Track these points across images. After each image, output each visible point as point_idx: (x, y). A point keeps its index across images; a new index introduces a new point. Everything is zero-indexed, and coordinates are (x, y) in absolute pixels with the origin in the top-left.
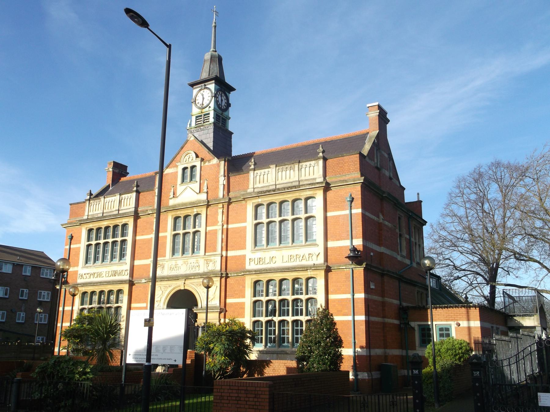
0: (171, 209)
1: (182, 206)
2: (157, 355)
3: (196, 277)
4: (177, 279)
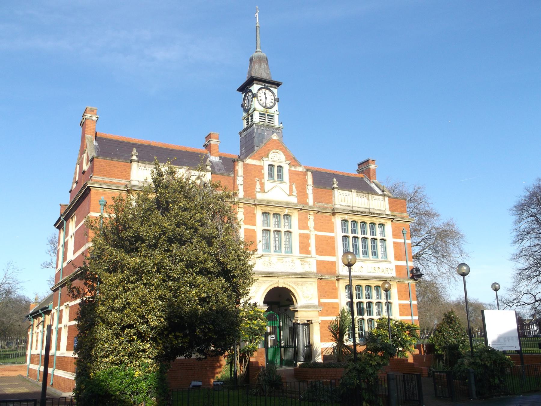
0: (265, 204)
1: (277, 204)
2: (505, 344)
3: (293, 276)
4: (276, 276)
